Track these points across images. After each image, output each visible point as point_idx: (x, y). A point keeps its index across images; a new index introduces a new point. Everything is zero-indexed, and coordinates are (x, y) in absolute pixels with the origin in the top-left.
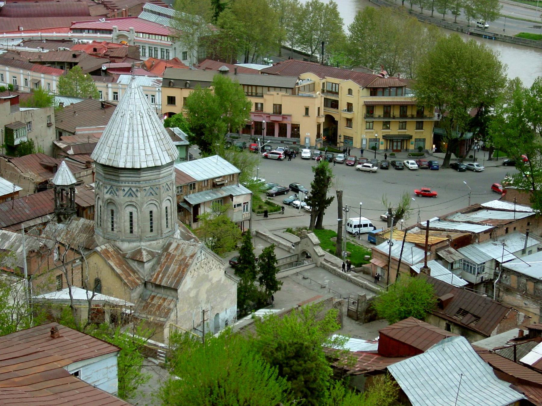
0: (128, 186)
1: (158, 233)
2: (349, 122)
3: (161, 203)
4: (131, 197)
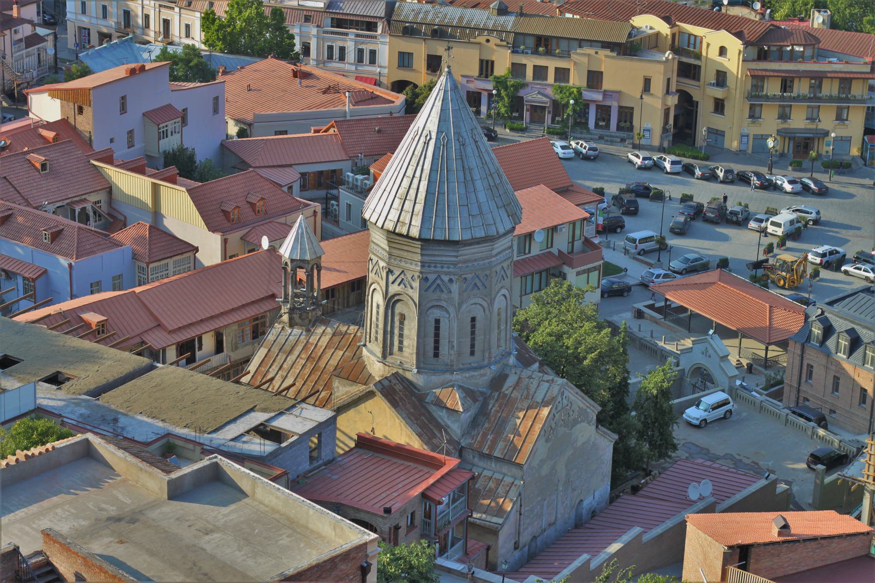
0: (435, 272)
1: (484, 356)
2: (719, 106)
3: (491, 303)
4: (438, 292)
